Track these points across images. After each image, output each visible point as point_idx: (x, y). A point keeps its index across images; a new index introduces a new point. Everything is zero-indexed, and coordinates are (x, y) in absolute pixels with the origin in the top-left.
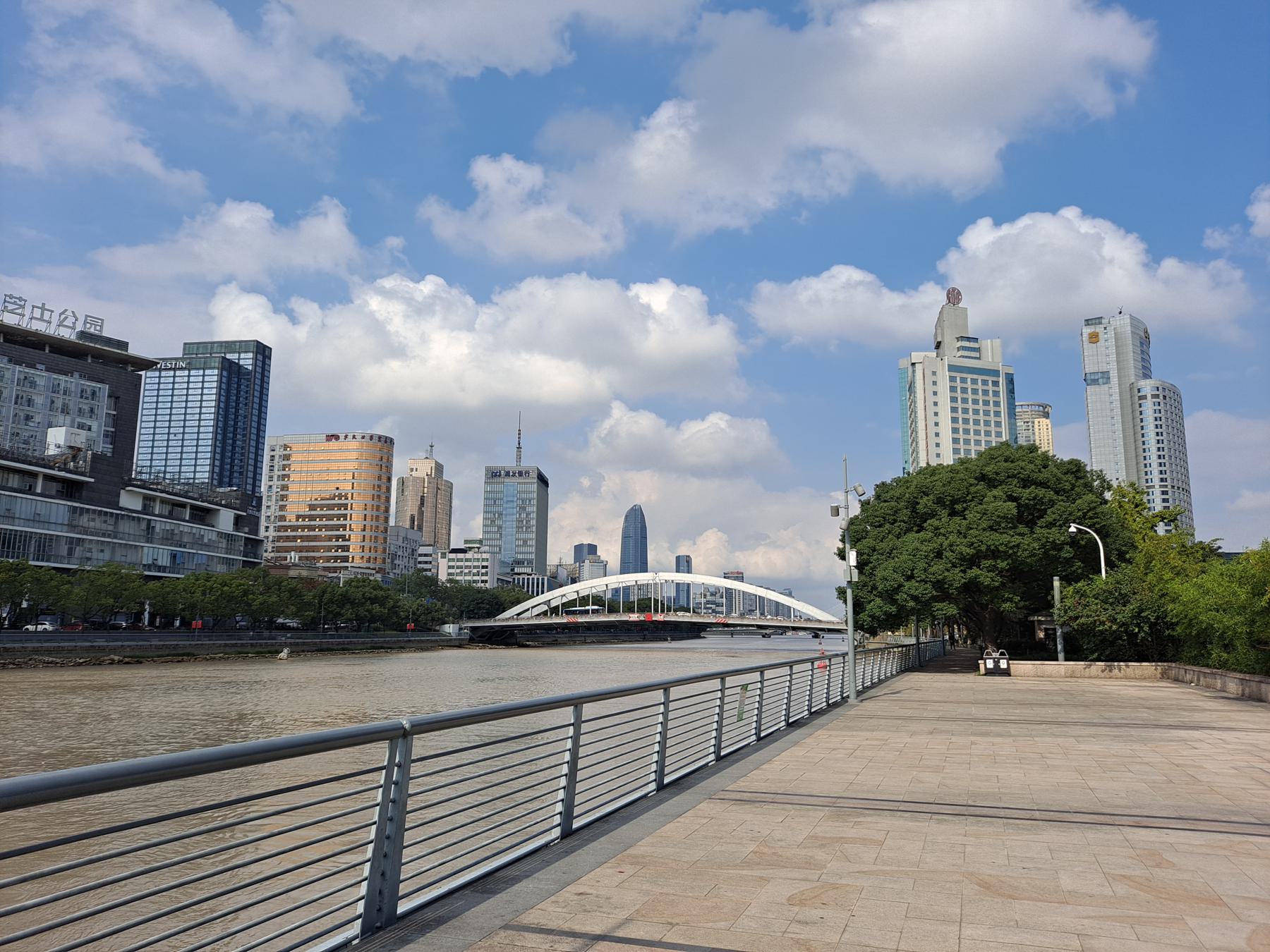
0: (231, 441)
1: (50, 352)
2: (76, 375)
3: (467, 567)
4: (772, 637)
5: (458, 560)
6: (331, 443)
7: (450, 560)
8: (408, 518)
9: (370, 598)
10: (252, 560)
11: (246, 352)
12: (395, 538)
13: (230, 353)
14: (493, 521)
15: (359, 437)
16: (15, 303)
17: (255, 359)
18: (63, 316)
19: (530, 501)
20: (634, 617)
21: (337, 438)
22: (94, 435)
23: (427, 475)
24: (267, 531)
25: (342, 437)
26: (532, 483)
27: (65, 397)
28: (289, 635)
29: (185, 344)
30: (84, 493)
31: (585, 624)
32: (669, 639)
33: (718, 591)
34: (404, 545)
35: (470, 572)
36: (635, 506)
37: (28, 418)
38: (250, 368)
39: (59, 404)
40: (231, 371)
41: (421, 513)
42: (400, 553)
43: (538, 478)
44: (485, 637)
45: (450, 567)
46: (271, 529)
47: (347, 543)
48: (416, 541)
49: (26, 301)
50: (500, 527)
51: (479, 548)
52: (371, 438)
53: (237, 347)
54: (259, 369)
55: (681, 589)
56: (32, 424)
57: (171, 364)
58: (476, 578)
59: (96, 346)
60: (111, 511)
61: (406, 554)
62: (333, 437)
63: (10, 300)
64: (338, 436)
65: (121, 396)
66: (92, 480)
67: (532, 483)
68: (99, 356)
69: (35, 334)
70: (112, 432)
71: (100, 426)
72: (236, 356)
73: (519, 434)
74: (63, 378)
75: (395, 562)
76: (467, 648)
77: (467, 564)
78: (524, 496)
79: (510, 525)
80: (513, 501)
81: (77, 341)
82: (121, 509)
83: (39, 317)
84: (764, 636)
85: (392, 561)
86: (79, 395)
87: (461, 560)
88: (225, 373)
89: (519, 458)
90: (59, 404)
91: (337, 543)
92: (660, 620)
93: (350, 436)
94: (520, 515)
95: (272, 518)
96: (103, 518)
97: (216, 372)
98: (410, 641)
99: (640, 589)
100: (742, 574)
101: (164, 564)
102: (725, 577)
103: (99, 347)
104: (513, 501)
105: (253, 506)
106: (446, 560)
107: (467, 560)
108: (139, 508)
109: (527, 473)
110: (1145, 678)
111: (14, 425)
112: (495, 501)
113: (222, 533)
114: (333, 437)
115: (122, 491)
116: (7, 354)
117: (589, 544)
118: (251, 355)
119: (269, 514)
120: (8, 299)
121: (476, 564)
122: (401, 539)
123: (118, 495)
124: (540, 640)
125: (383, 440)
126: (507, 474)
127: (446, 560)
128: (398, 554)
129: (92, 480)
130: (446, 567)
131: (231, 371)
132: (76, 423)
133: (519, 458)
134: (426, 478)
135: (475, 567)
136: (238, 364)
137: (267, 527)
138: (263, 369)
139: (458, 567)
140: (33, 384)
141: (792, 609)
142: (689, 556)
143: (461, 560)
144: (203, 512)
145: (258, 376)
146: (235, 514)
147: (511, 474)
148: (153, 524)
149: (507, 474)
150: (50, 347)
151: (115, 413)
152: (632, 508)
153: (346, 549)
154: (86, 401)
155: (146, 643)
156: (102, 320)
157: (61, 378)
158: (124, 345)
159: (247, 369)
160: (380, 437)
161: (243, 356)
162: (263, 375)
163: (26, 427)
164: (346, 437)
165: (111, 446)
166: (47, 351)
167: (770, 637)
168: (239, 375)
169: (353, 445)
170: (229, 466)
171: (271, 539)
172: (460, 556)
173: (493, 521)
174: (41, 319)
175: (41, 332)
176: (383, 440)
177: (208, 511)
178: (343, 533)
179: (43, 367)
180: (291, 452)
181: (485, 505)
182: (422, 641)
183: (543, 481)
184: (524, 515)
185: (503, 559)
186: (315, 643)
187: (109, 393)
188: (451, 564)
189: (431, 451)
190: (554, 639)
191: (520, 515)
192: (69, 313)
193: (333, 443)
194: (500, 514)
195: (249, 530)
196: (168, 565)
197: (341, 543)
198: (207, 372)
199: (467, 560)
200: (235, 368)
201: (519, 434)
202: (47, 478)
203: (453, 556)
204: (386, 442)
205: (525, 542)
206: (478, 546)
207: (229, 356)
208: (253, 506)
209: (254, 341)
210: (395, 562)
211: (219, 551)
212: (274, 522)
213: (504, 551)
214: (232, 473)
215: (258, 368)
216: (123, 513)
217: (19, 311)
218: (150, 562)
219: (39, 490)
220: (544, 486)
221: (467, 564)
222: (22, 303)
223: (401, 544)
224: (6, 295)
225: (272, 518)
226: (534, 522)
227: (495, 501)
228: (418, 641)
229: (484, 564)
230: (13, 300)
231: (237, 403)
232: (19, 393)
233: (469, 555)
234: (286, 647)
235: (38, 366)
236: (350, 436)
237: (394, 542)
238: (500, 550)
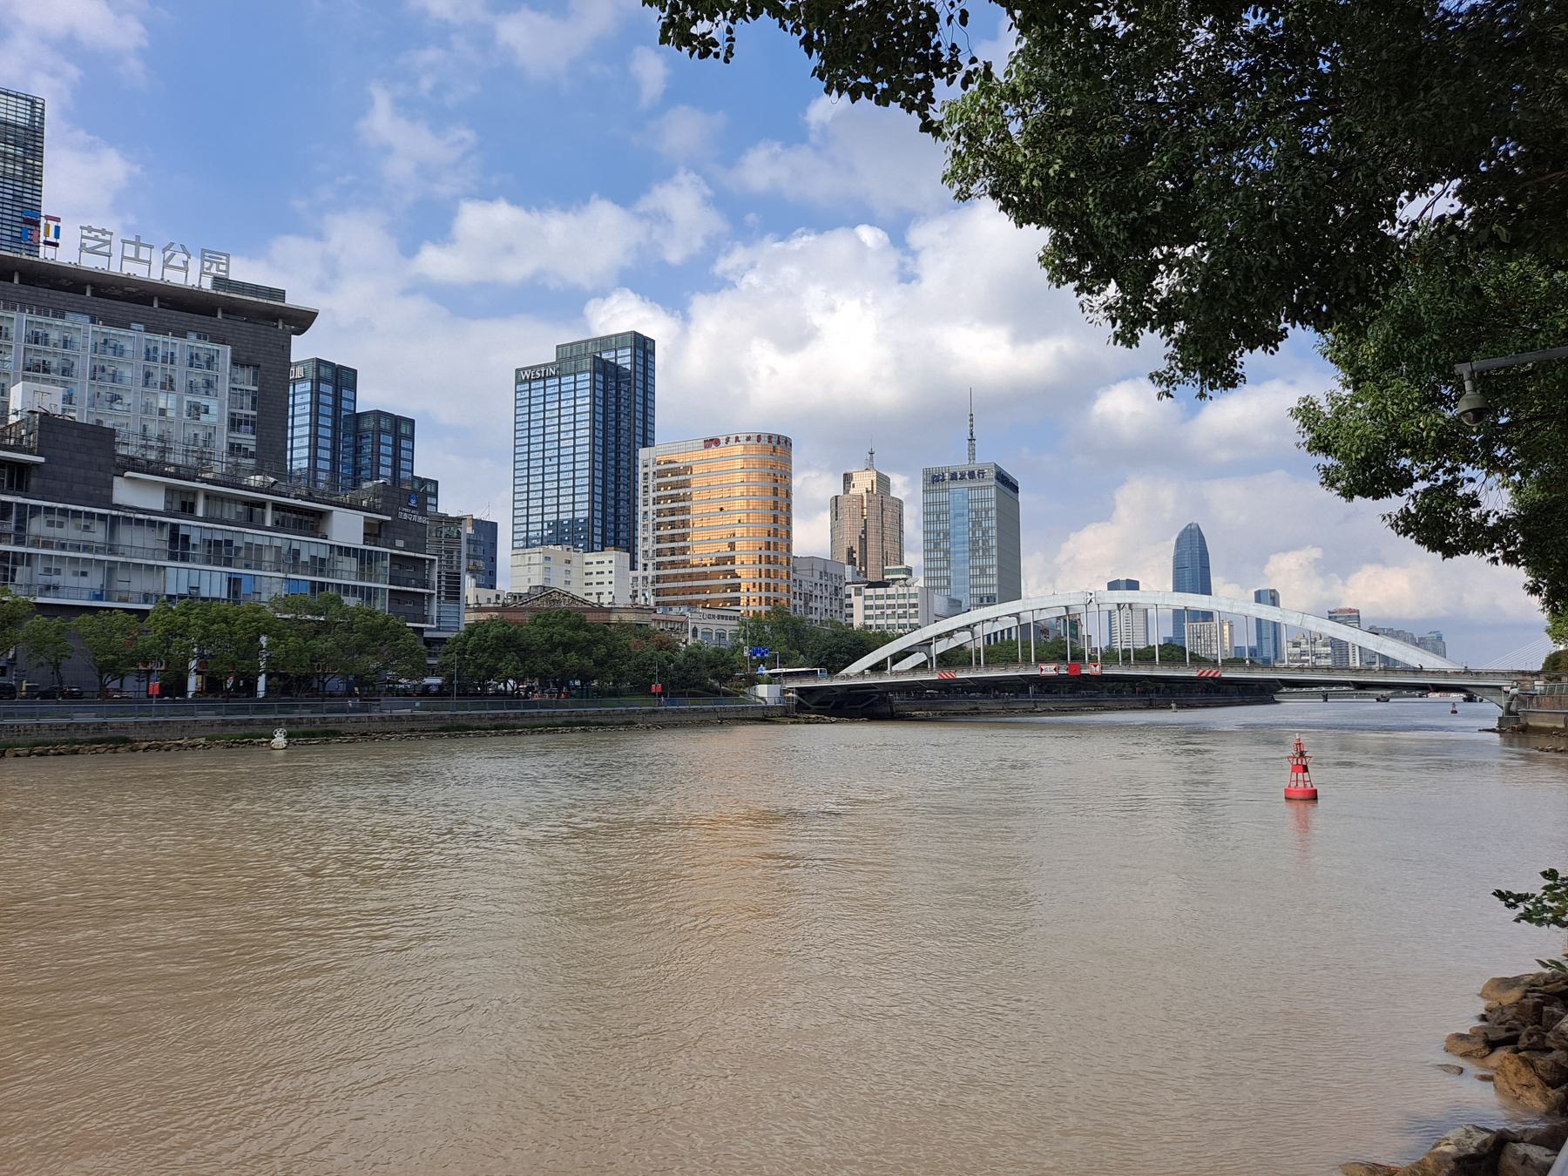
0: (613, 463)
1: (160, 306)
2: (193, 336)
3: (889, 606)
4: (1391, 700)
5: (878, 597)
6: (710, 450)
7: (866, 598)
8: (845, 551)
9: (560, 644)
10: (412, 589)
11: (623, 348)
12: (809, 573)
13: (606, 351)
14: (937, 544)
15: (743, 439)
16: (96, 238)
17: (634, 356)
18: (168, 253)
19: (987, 513)
20: (1049, 670)
21: (716, 442)
22: (214, 419)
23: (867, 492)
24: (645, 570)
25: (723, 441)
26: (988, 487)
27: (164, 365)
28: (417, 704)
29: (558, 347)
30: (33, 481)
31: (972, 683)
32: (1173, 705)
33: (1318, 637)
34: (823, 582)
35: (894, 613)
36: (1190, 525)
37: (115, 398)
38: (629, 367)
39: (158, 377)
40: (606, 373)
41: (863, 541)
42: (817, 592)
43: (997, 478)
44: (828, 703)
45: (866, 607)
46: (650, 567)
47: (737, 581)
48: (840, 577)
49: (111, 234)
50: (947, 552)
51: (905, 579)
52: (759, 439)
53: (613, 343)
54: (640, 369)
55: (1264, 636)
56: (119, 407)
57: (540, 372)
58: (891, 621)
59: (219, 293)
60: (87, 509)
61: (826, 594)
62: (712, 442)
63: (89, 235)
64: (718, 440)
65: (262, 364)
66: (42, 460)
67: (988, 487)
68: (234, 310)
69: (128, 281)
70: (253, 417)
71: (221, 406)
72: (613, 354)
73: (971, 420)
74: (160, 338)
75: (810, 604)
76: (778, 723)
77: (889, 602)
78: (976, 506)
79: (960, 550)
80: (963, 515)
81: (214, 292)
82: (118, 507)
83: (133, 256)
84: (1378, 700)
85: (806, 604)
86: (144, 356)
87: (882, 597)
88: (600, 377)
89: (972, 453)
90: (158, 377)
91: (725, 581)
92: (1095, 673)
93: (732, 440)
94: (974, 533)
95: (650, 554)
96: (83, 522)
97: (588, 376)
98: (655, 712)
99: (1200, 637)
100: (1358, 611)
101: (216, 594)
102: (1330, 618)
103: (223, 293)
104: (963, 515)
105: (413, 508)
106: (861, 598)
107: (889, 597)
108: (160, 506)
109: (981, 473)
110: (1477, 673)
111: (92, 410)
112: (938, 517)
113: (341, 547)
114: (712, 442)
115: (117, 480)
116: (87, 311)
117: (1127, 580)
118: (628, 351)
119: (646, 548)
120: (85, 233)
121: (901, 601)
122: (817, 574)
123: (110, 486)
124: (943, 708)
125: (774, 440)
126: (953, 477)
127: (861, 598)
128: (815, 593)
129: (42, 460)
130: (862, 608)
131: (606, 373)
132: (185, 403)
133: (972, 453)
134: (865, 495)
135: (900, 606)
136: (615, 364)
137: (645, 565)
138: (645, 367)
139: (878, 607)
140: (119, 351)
141: (1350, 646)
142: (1274, 591)
143: (882, 597)
144: (312, 515)
145: (640, 377)
146: (365, 517)
147: (959, 476)
148: (183, 531)
149: (953, 477)
150: (160, 300)
151: (256, 388)
152: (1186, 529)
153: (736, 588)
154: (199, 371)
155: (27, 721)
156: (558, 347)
157: (157, 338)
158: (280, 294)
159: (626, 369)
160: (770, 437)
161: (620, 353)
162: (645, 375)
163: (110, 412)
164: (728, 440)
165: (254, 437)
166: (156, 306)
167: (1388, 701)
168: (617, 378)
169: (738, 449)
170: (613, 494)
171: (650, 580)
172: (880, 591)
173: (937, 544)
174: (136, 259)
175: (102, 272)
176: (774, 440)
177: (322, 515)
178: (732, 567)
179: (142, 327)
180: (691, 476)
181: (926, 523)
182: (683, 712)
183: (1007, 483)
184: (979, 534)
185: (953, 596)
186: (441, 718)
187: (232, 359)
188: (869, 603)
189: (872, 459)
190: (973, 706)
191: (974, 533)
192: (176, 247)
193: (714, 451)
194: (947, 534)
195: (406, 544)
196: (225, 596)
197: (730, 581)
198: (579, 377)
199: (889, 597)
200: (611, 370)
201: (971, 420)
202: (277, 507)
203: (870, 592)
204: (779, 443)
205: (983, 569)
206: (904, 576)
207: (605, 356)
208: (413, 508)
209: (630, 333)
210: (810, 604)
211: (339, 576)
212: (653, 558)
213: (955, 584)
214: (617, 501)
215: (638, 367)
216: (114, 513)
217: (105, 249)
218: (184, 591)
219: (268, 523)
220: (1007, 490)
221: (889, 602)
222: (107, 237)
223: (819, 582)
224: (82, 228)
225: (650, 554)
226: (993, 542)
227: (938, 517)
228: (674, 712)
229: (913, 601)
230: (93, 234)
231: (618, 415)
232: (97, 363)
233: (891, 590)
234: (279, 725)
235: (134, 326)
236: (732, 440)
237: (807, 578)
238: (949, 583)
